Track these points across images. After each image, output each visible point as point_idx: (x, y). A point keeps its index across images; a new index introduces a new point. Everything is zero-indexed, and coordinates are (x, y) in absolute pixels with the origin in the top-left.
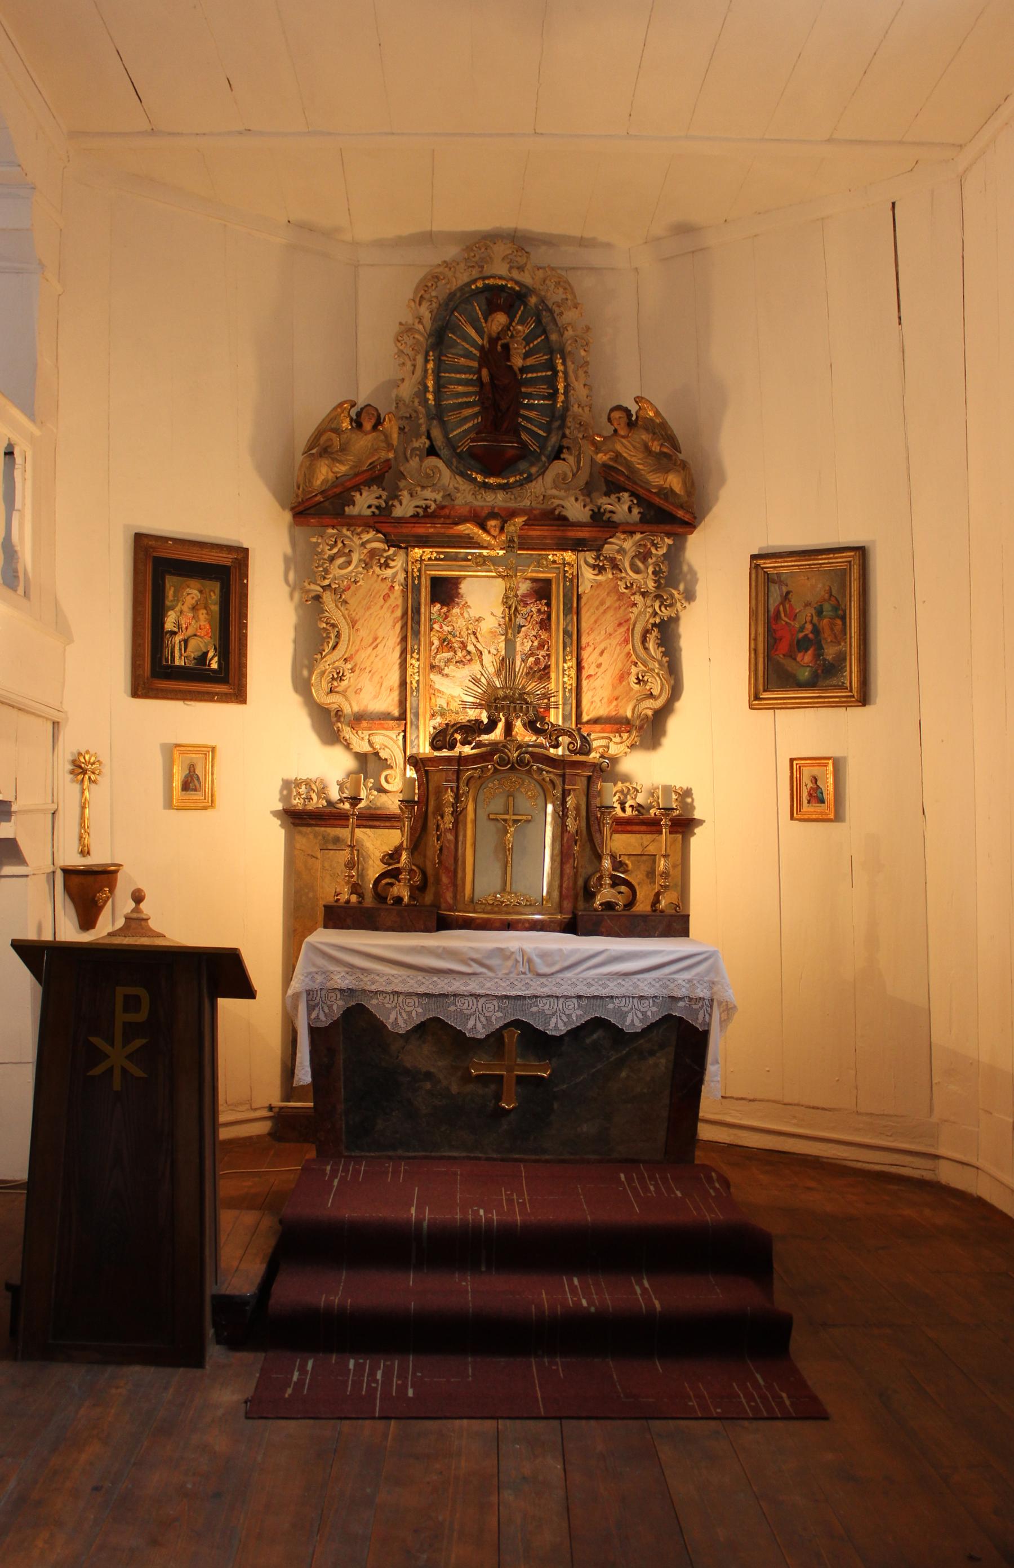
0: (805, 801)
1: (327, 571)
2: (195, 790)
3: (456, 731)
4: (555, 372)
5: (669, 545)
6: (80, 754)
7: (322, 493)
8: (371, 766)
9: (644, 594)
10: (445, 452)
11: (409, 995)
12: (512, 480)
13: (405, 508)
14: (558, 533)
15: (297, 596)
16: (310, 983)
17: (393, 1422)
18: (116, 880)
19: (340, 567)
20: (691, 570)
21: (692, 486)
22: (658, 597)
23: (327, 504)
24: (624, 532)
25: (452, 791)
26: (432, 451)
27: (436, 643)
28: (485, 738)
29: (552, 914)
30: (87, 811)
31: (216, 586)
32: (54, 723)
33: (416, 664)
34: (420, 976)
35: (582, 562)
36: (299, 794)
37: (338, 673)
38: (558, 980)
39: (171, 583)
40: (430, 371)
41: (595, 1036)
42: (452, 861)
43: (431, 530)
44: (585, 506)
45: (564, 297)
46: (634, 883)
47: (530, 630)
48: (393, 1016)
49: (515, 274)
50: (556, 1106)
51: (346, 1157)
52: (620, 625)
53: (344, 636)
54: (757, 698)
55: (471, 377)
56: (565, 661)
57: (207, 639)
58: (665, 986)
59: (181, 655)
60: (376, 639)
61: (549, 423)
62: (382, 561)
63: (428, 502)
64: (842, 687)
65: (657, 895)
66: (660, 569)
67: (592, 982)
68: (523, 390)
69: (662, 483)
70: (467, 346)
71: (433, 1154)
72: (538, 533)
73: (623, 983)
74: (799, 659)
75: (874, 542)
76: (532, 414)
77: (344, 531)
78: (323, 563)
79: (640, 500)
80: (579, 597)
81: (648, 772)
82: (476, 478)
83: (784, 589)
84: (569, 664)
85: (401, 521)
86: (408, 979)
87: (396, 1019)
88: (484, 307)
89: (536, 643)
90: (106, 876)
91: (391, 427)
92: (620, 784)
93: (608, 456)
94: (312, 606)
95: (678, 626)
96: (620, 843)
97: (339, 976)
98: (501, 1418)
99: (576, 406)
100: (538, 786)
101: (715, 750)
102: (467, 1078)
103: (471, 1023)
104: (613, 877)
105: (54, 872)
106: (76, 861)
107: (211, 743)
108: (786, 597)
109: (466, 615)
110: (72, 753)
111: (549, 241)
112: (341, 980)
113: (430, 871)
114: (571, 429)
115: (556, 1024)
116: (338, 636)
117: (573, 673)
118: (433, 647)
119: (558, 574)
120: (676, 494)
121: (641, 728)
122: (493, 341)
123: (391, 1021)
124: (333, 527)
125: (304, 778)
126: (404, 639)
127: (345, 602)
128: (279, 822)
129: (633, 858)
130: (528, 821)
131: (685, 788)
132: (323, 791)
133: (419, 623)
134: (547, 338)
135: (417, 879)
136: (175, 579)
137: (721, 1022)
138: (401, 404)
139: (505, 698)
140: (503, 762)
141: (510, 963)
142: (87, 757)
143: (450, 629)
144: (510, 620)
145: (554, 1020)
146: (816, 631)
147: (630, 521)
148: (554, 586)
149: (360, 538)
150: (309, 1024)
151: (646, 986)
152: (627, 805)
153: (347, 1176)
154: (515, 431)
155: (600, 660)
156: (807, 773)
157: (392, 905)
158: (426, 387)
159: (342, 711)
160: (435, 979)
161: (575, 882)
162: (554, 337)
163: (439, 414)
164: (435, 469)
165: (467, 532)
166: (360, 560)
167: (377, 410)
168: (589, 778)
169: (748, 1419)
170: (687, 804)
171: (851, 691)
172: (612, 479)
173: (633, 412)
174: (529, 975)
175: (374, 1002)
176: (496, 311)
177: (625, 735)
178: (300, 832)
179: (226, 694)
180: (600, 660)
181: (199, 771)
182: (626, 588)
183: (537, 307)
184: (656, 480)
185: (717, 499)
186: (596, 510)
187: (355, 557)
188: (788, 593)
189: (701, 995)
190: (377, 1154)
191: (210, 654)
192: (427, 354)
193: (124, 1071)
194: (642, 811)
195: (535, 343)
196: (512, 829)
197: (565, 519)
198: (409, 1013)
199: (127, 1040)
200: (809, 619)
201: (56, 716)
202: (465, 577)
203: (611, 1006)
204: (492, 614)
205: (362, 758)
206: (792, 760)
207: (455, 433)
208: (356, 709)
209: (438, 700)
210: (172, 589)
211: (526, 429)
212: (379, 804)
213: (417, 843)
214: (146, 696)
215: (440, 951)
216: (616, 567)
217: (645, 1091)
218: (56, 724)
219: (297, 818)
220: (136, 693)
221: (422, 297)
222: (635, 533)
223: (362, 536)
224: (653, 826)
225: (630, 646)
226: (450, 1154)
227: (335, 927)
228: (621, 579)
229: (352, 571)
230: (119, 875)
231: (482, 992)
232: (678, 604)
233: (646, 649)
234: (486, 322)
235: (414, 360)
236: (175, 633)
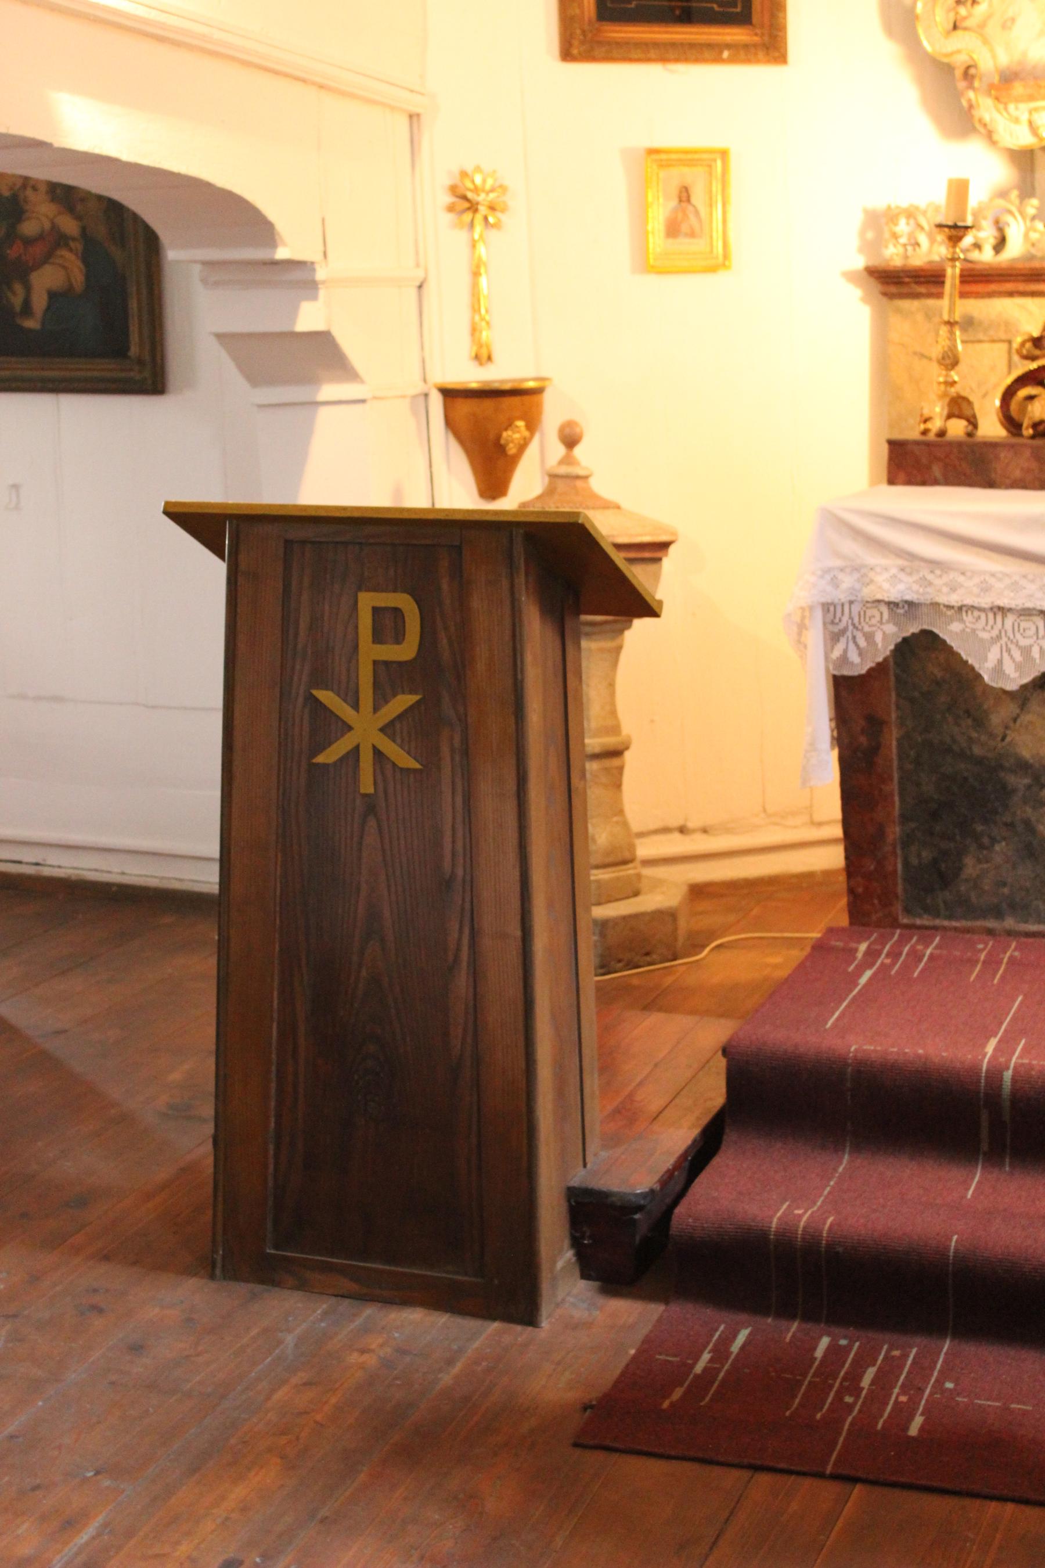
2: (692, 234)
6: (464, 174)
11: (1026, 613)
16: (829, 588)
17: (858, 1488)
18: (539, 406)
30: (483, 281)
32: (411, 116)
36: (895, 236)
48: (993, 655)
86: (1023, 582)
87: (1000, 662)
90: (516, 400)
97: (886, 575)
105: (426, 395)
106: (473, 376)
107: (718, 144)
125: (904, 205)
142: (478, 179)
150: (827, 669)
153: (894, 964)
157: (1033, 437)
159: (975, 66)
175: (956, 627)
178: (898, 311)
179: (746, 47)
193: (378, 753)
198: (1026, 651)
199: (381, 699)
208: (1004, 59)
214: (589, 56)
218: (413, 117)
220: (567, 54)
227: (910, 482)
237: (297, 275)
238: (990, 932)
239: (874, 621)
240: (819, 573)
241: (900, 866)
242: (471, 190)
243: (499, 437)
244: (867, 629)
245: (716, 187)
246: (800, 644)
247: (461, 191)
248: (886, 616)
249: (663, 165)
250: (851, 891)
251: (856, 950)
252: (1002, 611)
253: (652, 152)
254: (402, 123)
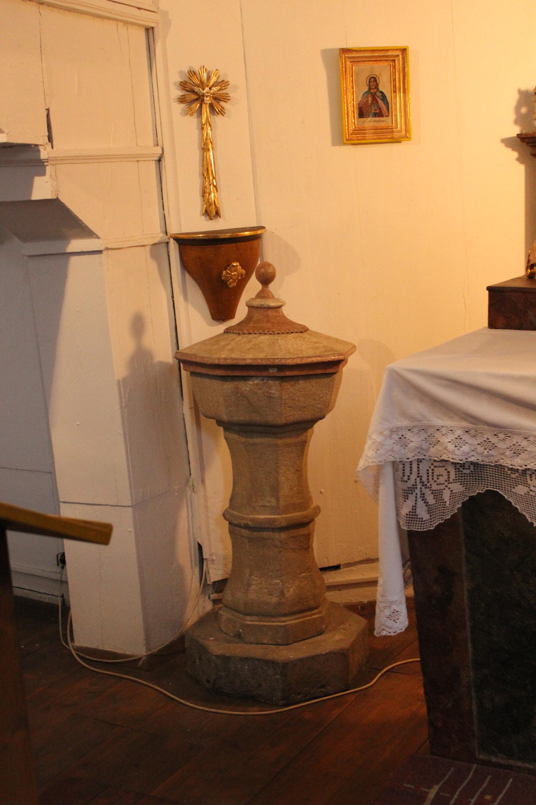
16: (397, 448)
51: (483, 762)
97: (451, 437)
105: (168, 243)
106: (197, 225)
107: (401, 44)
110: (181, 72)
112: (453, 446)
128: (515, 155)
175: (521, 490)
181: (385, 87)
201: (149, 19)
218: (149, 31)
237: (25, 156)
239: (442, 480)
240: (387, 433)
241: (474, 707)
242: (198, 86)
244: (435, 487)
248: (452, 476)
249: (355, 61)
250: (431, 723)
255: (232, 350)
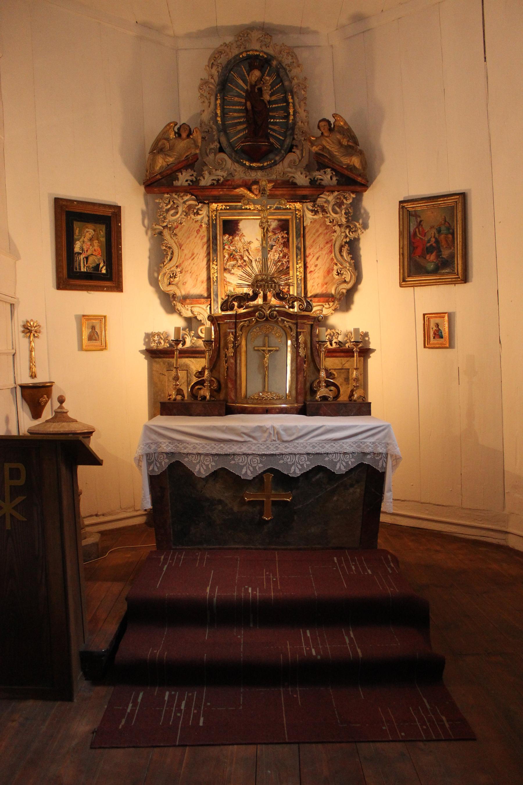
0: (432, 337)
1: (165, 218)
2: (96, 340)
3: (233, 300)
4: (288, 103)
5: (353, 198)
6: (27, 322)
7: (160, 174)
8: (194, 324)
9: (340, 226)
10: (228, 150)
11: (207, 455)
12: (265, 164)
13: (206, 181)
14: (292, 192)
15: (150, 233)
17: (187, 748)
19: (172, 215)
20: (366, 212)
21: (365, 164)
22: (348, 227)
23: (163, 180)
24: (328, 191)
25: (232, 334)
26: (221, 150)
27: (227, 256)
28: (252, 303)
29: (292, 404)
30: (33, 353)
31: (103, 227)
32: (11, 305)
33: (216, 267)
34: (213, 444)
35: (305, 209)
36: (154, 340)
37: (173, 274)
38: (295, 444)
39: (77, 226)
40: (218, 105)
41: (318, 477)
42: (233, 375)
43: (221, 193)
44: (306, 177)
45: (292, 61)
46: (338, 385)
47: (278, 248)
49: (264, 49)
50: (296, 517)
52: (327, 243)
53: (176, 254)
54: (404, 281)
55: (241, 108)
56: (297, 264)
57: (99, 257)
58: (359, 447)
59: (84, 265)
60: (193, 254)
61: (285, 132)
62: (195, 211)
63: (219, 177)
64: (452, 273)
65: (352, 391)
66: (349, 211)
67: (316, 445)
68: (271, 114)
69: (349, 162)
70: (239, 91)
71: (225, 547)
72: (281, 192)
73: (334, 445)
74: (427, 258)
75: (470, 190)
76: (276, 128)
77: (174, 195)
78: (163, 214)
79: (337, 172)
80: (304, 228)
81: (343, 324)
82: (245, 164)
83: (419, 219)
84: (300, 265)
85: (204, 188)
86: (206, 446)
87: (200, 469)
88: (247, 68)
89: (281, 255)
91: (197, 136)
92: (329, 330)
93: (318, 148)
94: (158, 238)
95: (359, 243)
96: (330, 363)
98: (260, 744)
99: (300, 122)
100: (282, 330)
101: (381, 310)
102: (243, 503)
103: (244, 471)
104: (326, 382)
105: (16, 388)
106: (27, 380)
107: (104, 314)
108: (420, 224)
109: (242, 240)
111: (282, 30)
112: (166, 447)
113: (222, 381)
114: (298, 136)
115: (295, 470)
116: (172, 253)
117: (302, 270)
118: (225, 259)
119: (292, 217)
120: (357, 168)
121: (340, 299)
122: (253, 87)
123: (197, 470)
124: (168, 193)
125: (157, 332)
126: (209, 254)
127: (176, 235)
128: (144, 356)
129: (337, 371)
130: (277, 351)
131: (364, 332)
132: (166, 339)
133: (216, 245)
134: (283, 84)
135: (215, 385)
136: (79, 223)
137: (392, 466)
138: (203, 125)
139: (262, 280)
140: (261, 317)
141: (266, 435)
142: (32, 323)
143: (234, 248)
144: (264, 235)
145: (293, 468)
146: (437, 241)
147: (332, 184)
148: (290, 223)
149: (183, 199)
150: (148, 473)
151: (348, 446)
152: (333, 342)
154: (267, 136)
155: (317, 262)
156: (433, 322)
157: (201, 400)
158: (216, 114)
159: (176, 294)
160: (222, 445)
161: (305, 384)
162: (286, 83)
163: (224, 129)
164: (223, 160)
165: (240, 193)
166: (183, 211)
167: (189, 126)
168: (312, 325)
169: (422, 741)
170: (366, 340)
171: (458, 275)
172: (321, 161)
173: (332, 122)
174: (278, 442)
175: (186, 459)
176: (254, 69)
177: (331, 304)
178: (155, 361)
179: (111, 287)
180: (317, 262)
182: (330, 222)
183: (276, 66)
184: (345, 160)
185: (379, 171)
186: (313, 179)
187: (180, 210)
188: (421, 221)
189: (381, 451)
190: (192, 547)
191: (101, 265)
192: (216, 96)
193: (12, 516)
194: (341, 345)
195: (276, 87)
196: (268, 355)
197: (295, 184)
200: (433, 235)
201: (12, 301)
202: (241, 220)
203: (327, 459)
204: (257, 239)
205: (189, 320)
206: (424, 315)
207: (233, 139)
208: (183, 293)
209: (229, 287)
210: (78, 229)
211: (272, 135)
212: (197, 345)
213: (214, 366)
215: (224, 428)
216: (324, 211)
217: (348, 507)
218: (12, 305)
219: (153, 354)
221: (212, 63)
222: (334, 191)
223: (184, 198)
224: (349, 353)
225: (333, 254)
226: (234, 546)
228: (327, 217)
229: (179, 218)
230: (53, 387)
231: (250, 452)
232: (359, 231)
233: (342, 256)
234: (248, 75)
235: (210, 99)
236: (81, 254)
238: (199, 549)
241: (172, 531)
243: (39, 400)
244: (160, 461)
245: (103, 326)
246: (139, 466)
247: (27, 326)
251: (160, 558)
252: (199, 454)
253: (84, 316)
254: (9, 306)
255: (54, 428)
